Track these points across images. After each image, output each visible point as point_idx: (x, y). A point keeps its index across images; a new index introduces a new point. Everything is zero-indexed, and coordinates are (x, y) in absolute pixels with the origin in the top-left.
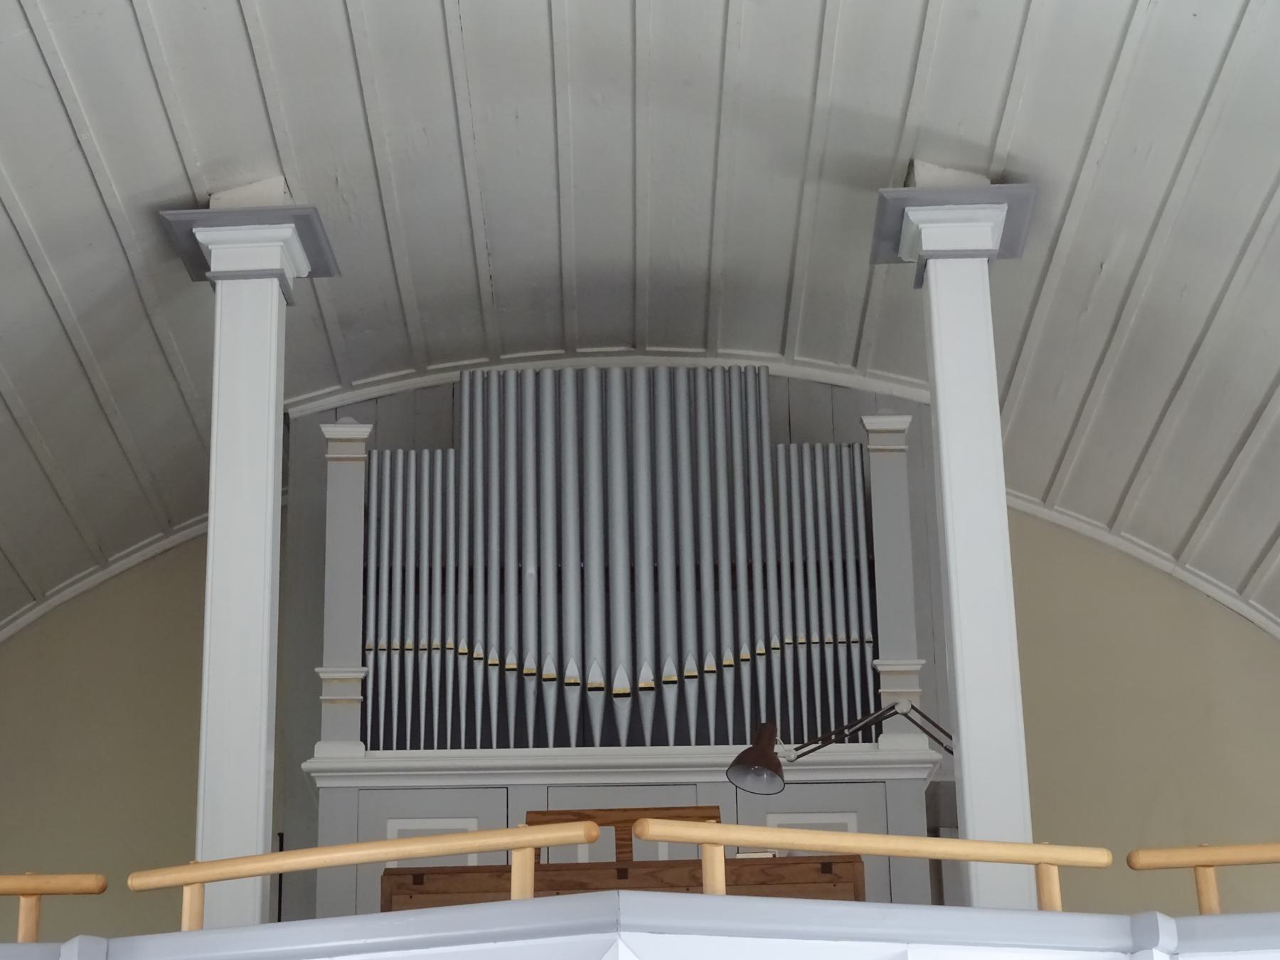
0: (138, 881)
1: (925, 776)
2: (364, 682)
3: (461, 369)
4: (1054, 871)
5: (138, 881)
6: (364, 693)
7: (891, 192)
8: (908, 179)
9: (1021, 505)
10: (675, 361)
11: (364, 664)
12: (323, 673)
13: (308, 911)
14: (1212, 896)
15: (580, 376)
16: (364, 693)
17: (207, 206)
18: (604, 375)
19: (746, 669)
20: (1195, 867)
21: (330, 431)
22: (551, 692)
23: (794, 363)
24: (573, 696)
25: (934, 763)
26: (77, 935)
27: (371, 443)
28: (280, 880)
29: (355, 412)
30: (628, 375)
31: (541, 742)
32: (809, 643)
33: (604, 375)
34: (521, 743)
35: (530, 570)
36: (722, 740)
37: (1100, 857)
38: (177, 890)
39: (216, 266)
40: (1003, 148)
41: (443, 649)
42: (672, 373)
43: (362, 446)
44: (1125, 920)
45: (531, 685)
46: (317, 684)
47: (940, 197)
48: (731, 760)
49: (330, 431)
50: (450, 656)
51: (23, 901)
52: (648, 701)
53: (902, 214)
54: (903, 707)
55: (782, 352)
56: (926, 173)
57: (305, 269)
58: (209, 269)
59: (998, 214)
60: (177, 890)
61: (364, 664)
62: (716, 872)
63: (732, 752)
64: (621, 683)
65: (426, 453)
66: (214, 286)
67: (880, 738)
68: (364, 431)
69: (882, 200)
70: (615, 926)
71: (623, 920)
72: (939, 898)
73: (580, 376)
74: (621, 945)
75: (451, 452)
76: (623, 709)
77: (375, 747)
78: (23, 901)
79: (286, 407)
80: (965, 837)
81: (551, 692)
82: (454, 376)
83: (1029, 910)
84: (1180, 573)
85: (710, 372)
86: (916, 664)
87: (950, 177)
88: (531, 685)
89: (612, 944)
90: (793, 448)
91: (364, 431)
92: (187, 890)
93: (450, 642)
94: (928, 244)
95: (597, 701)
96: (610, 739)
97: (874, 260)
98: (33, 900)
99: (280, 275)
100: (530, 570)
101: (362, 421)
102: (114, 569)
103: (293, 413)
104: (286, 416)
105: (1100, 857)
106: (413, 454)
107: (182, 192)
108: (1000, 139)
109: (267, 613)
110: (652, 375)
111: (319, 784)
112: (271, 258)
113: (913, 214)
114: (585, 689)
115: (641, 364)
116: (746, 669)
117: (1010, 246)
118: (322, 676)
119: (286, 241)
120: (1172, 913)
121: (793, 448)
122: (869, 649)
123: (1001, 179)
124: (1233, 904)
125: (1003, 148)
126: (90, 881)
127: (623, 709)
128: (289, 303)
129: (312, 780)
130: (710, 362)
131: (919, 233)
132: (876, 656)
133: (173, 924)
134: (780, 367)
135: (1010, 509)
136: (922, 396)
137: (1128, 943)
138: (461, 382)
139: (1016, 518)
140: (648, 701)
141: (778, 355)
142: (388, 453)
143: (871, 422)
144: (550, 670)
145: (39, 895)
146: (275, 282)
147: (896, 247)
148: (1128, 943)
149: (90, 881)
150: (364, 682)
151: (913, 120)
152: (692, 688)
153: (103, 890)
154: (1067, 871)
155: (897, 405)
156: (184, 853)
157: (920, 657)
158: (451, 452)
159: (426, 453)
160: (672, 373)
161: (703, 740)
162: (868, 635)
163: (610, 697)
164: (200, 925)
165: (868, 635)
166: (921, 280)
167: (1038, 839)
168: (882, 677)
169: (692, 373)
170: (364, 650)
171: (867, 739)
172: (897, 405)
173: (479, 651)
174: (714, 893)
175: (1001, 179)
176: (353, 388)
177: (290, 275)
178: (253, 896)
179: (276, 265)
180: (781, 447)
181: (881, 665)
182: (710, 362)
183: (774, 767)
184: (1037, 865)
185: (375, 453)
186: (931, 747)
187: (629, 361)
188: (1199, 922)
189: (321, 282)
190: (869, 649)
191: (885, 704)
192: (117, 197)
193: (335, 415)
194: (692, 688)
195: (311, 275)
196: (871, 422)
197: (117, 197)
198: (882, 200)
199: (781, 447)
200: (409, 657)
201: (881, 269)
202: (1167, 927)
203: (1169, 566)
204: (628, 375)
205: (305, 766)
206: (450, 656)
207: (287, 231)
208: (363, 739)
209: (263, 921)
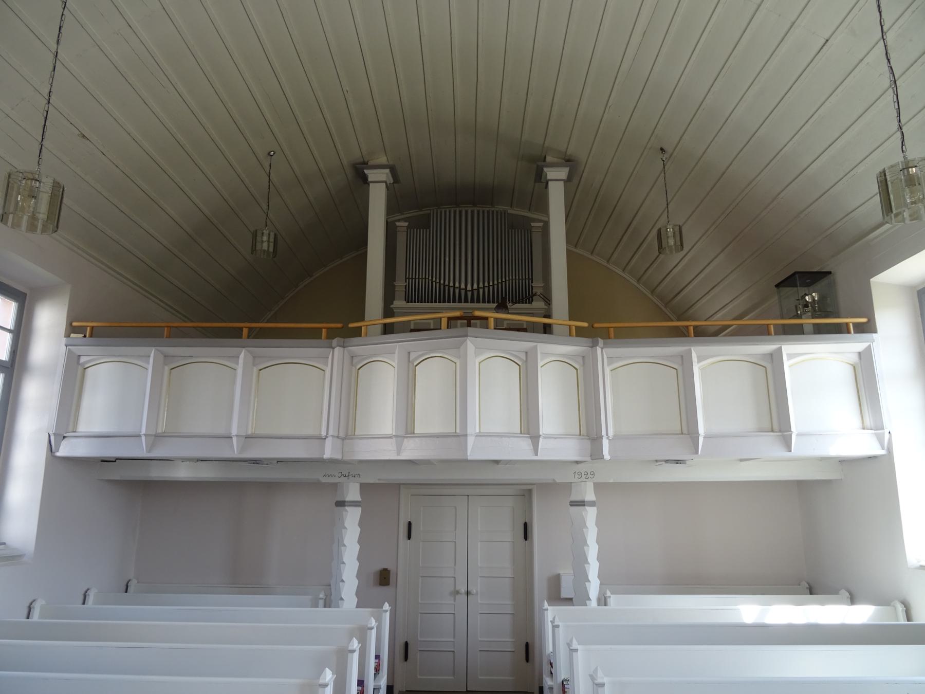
0: (351, 325)
1: (543, 312)
2: (406, 286)
3: (431, 210)
4: (574, 327)
5: (351, 325)
6: (406, 289)
7: (539, 163)
8: (544, 160)
9: (569, 248)
10: (484, 209)
11: (406, 282)
12: (396, 284)
13: (392, 332)
14: (612, 335)
15: (460, 212)
16: (406, 289)
17: (367, 164)
18: (466, 212)
19: (500, 285)
20: (608, 328)
21: (398, 224)
22: (452, 290)
23: (514, 210)
24: (457, 291)
25: (545, 309)
26: (336, 338)
27: (408, 227)
28: (385, 325)
29: (405, 220)
30: (473, 212)
31: (449, 302)
32: (516, 279)
33: (466, 212)
34: (444, 302)
35: (447, 259)
36: (493, 302)
37: (585, 324)
38: (360, 327)
39: (369, 180)
40: (569, 152)
41: (425, 279)
42: (483, 212)
43: (406, 228)
44: (590, 340)
45: (447, 288)
46: (394, 286)
47: (552, 165)
48: (494, 307)
49: (398, 224)
50: (427, 280)
51: (323, 330)
52: (475, 293)
53: (543, 169)
54: (538, 294)
55: (511, 207)
56: (549, 159)
57: (392, 182)
58: (367, 180)
59: (567, 170)
60: (360, 327)
61: (406, 282)
62: (492, 323)
63: (495, 305)
64: (469, 288)
65: (422, 230)
66: (369, 185)
67: (533, 303)
68: (406, 224)
69: (538, 166)
70: (466, 336)
71: (469, 334)
72: (545, 332)
73: (460, 212)
74: (468, 340)
75: (428, 230)
76: (469, 294)
77: (408, 302)
78: (323, 330)
79: (387, 219)
80: (552, 318)
81: (452, 290)
82: (429, 211)
83: (567, 336)
84: (608, 266)
85: (493, 212)
86: (542, 285)
87: (555, 160)
88: (447, 288)
89: (466, 340)
90: (513, 231)
91: (406, 224)
92: (363, 327)
93: (427, 277)
94: (549, 177)
95: (463, 292)
96: (466, 301)
97: (535, 182)
98: (326, 329)
99: (386, 182)
100: (447, 259)
101: (406, 221)
102: (344, 260)
103: (389, 220)
104: (387, 222)
105: (585, 324)
106: (418, 230)
107: (361, 160)
108: (568, 150)
109: (381, 296)
110: (478, 212)
111: (395, 311)
112: (384, 178)
113: (545, 169)
114: (460, 288)
115: (476, 210)
116: (500, 285)
117: (568, 180)
118: (396, 284)
119: (387, 174)
120: (602, 338)
121: (513, 231)
122: (530, 281)
123: (568, 161)
124: (617, 336)
125: (569, 152)
126: (339, 325)
127: (469, 294)
128: (388, 190)
129: (393, 310)
130: (493, 209)
131: (546, 175)
132: (532, 282)
133: (360, 335)
134: (510, 211)
135: (567, 249)
136: (545, 219)
137: (591, 345)
138: (431, 213)
139: (568, 251)
140: (475, 293)
141: (510, 208)
142: (412, 230)
143: (533, 224)
144: (451, 284)
145: (328, 328)
146: (384, 184)
147: (541, 178)
148: (591, 345)
149: (339, 325)
150: (406, 286)
151: (547, 144)
152: (486, 289)
153: (343, 327)
154: (577, 327)
155: (540, 221)
156: (362, 319)
157: (543, 283)
158: (428, 230)
159: (422, 230)
160: (483, 212)
161: (489, 302)
162: (530, 277)
163: (466, 291)
164: (366, 335)
165: (530, 277)
166: (547, 186)
167: (570, 320)
168: (534, 288)
169: (488, 212)
170: (406, 278)
171: (529, 303)
172: (540, 221)
173: (434, 279)
174: (491, 329)
175: (568, 161)
176: (403, 214)
177: (388, 183)
178: (379, 328)
179: (385, 180)
180: (510, 230)
181: (534, 285)
182: (493, 209)
183: (507, 308)
184: (570, 326)
185: (409, 230)
186: (545, 305)
187: (473, 208)
188: (609, 341)
189: (395, 185)
190: (530, 281)
191: (534, 293)
192: (345, 162)
193: (399, 220)
194: (486, 289)
195: (393, 183)
196: (533, 224)
197: (345, 162)
198: (538, 166)
199: (510, 230)
200: (417, 280)
201: (537, 184)
202: (601, 341)
203: (606, 264)
204: (473, 212)
205: (391, 306)
206: (427, 280)
207: (388, 171)
208: (405, 300)
209: (381, 335)
